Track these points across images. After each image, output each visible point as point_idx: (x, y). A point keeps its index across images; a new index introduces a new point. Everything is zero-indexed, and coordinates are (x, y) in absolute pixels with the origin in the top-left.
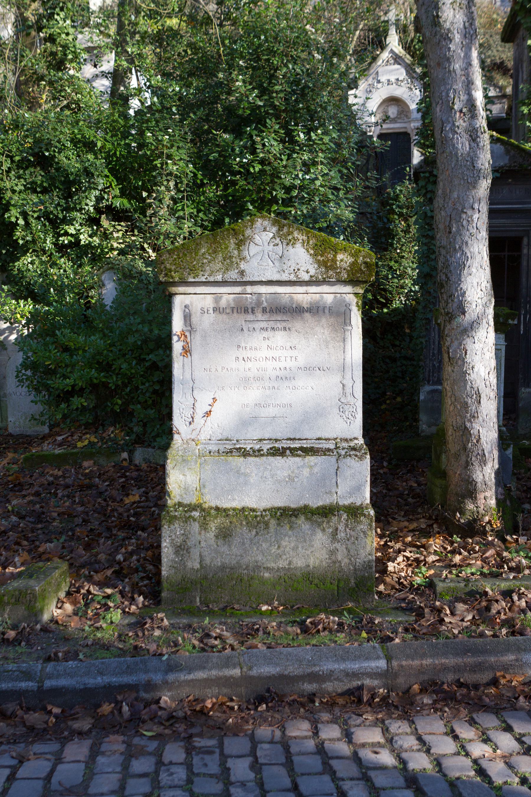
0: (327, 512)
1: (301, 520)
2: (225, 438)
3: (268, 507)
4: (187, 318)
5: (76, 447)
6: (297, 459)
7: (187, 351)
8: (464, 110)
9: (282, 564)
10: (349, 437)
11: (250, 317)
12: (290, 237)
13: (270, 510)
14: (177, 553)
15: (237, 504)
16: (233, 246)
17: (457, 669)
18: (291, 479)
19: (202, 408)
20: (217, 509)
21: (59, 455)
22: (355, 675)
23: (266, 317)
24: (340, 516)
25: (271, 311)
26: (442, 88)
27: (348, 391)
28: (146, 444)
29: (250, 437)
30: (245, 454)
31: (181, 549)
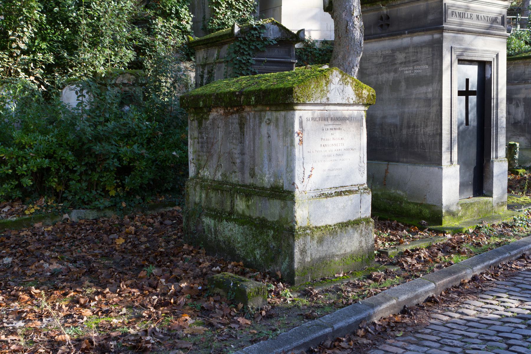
1: (349, 228)
2: (316, 189)
3: (335, 223)
4: (301, 123)
5: (25, 214)
6: (346, 197)
7: (301, 141)
8: (358, 17)
9: (342, 252)
10: (362, 183)
11: (326, 123)
12: (346, 81)
13: (337, 224)
14: (301, 254)
15: (323, 224)
16: (324, 84)
17: (450, 282)
18: (344, 207)
19: (307, 173)
20: (316, 227)
21: (15, 222)
22: (426, 292)
23: (333, 122)
24: (363, 223)
26: (347, 4)
27: (362, 160)
28: (78, 207)
29: (327, 186)
30: (327, 196)
31: (303, 252)
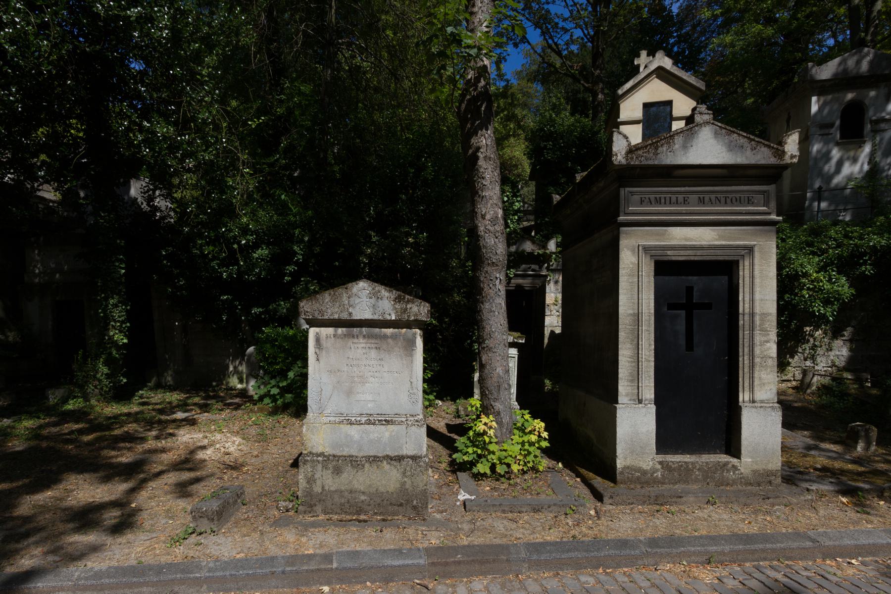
0: (400, 459)
11: (356, 340)
23: (364, 341)
25: (369, 337)
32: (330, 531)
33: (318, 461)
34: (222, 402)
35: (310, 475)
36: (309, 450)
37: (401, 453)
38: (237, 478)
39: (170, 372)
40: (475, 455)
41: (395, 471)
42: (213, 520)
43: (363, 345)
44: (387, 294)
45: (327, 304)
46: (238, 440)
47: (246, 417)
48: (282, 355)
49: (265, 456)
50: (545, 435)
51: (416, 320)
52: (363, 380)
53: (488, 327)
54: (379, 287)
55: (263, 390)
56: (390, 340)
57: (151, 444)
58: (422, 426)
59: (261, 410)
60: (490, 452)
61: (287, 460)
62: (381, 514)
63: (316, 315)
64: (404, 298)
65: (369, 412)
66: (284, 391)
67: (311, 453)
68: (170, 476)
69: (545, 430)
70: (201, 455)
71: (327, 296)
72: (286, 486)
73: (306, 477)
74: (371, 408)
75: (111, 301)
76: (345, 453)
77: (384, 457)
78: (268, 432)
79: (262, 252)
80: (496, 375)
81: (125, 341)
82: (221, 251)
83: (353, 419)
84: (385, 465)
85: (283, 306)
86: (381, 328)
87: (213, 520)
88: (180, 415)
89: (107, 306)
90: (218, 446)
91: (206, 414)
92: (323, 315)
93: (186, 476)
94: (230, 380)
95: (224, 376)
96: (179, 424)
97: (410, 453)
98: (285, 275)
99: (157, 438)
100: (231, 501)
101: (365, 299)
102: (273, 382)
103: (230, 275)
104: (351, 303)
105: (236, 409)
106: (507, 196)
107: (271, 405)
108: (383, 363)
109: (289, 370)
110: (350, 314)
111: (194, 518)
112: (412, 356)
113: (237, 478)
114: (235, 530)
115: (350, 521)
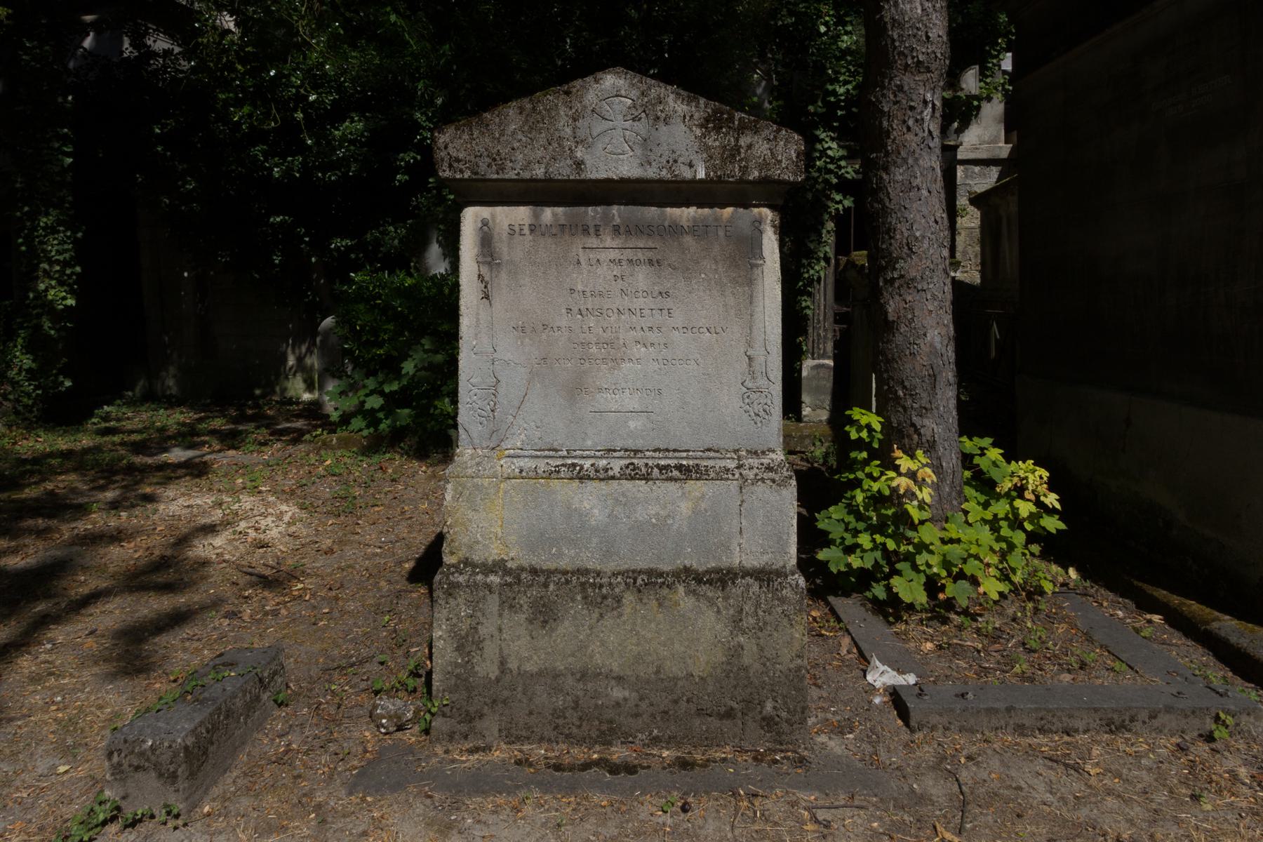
0: (723, 578)
11: (592, 241)
25: (629, 232)
32: (528, 810)
33: (489, 587)
34: (267, 427)
35: (464, 627)
36: (462, 554)
37: (725, 562)
38: (275, 613)
39: (172, 370)
40: (878, 554)
41: (710, 615)
42: (173, 777)
43: (614, 254)
44: (681, 108)
45: (511, 140)
46: (289, 510)
47: (313, 458)
48: (391, 327)
49: (349, 552)
50: (1052, 499)
51: (765, 181)
52: (614, 353)
53: (903, 227)
54: (658, 90)
55: (350, 403)
56: (688, 240)
57: (98, 520)
58: (783, 483)
59: (344, 443)
60: (923, 547)
61: (400, 563)
62: (670, 741)
63: (483, 168)
64: (731, 119)
65: (630, 444)
66: (393, 402)
67: (467, 562)
68: (109, 607)
69: (1051, 489)
70: (203, 548)
71: (512, 117)
72: (399, 642)
73: (453, 632)
74: (635, 431)
75: (43, 221)
76: (563, 564)
77: (676, 574)
78: (357, 492)
79: (354, 126)
80: (925, 349)
81: (71, 302)
82: (267, 115)
83: (587, 464)
84: (681, 596)
85: (394, 235)
86: (662, 205)
87: (173, 777)
88: (177, 455)
89: (35, 228)
90: (243, 524)
91: (232, 452)
92: (501, 169)
93: (154, 605)
94: (289, 385)
95: (278, 376)
96: (170, 473)
97: (752, 562)
98: (397, 170)
99: (115, 505)
100: (239, 703)
101: (620, 123)
102: (371, 383)
103: (288, 173)
104: (581, 133)
105: (296, 441)
106: (826, 24)
107: (365, 433)
108: (669, 303)
109: (405, 357)
110: (579, 164)
111: (117, 769)
112: (750, 282)
113: (275, 613)
114: (245, 803)
115: (586, 766)
